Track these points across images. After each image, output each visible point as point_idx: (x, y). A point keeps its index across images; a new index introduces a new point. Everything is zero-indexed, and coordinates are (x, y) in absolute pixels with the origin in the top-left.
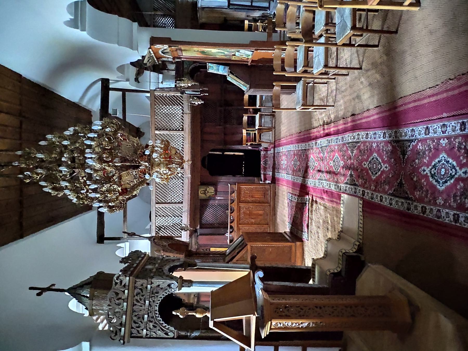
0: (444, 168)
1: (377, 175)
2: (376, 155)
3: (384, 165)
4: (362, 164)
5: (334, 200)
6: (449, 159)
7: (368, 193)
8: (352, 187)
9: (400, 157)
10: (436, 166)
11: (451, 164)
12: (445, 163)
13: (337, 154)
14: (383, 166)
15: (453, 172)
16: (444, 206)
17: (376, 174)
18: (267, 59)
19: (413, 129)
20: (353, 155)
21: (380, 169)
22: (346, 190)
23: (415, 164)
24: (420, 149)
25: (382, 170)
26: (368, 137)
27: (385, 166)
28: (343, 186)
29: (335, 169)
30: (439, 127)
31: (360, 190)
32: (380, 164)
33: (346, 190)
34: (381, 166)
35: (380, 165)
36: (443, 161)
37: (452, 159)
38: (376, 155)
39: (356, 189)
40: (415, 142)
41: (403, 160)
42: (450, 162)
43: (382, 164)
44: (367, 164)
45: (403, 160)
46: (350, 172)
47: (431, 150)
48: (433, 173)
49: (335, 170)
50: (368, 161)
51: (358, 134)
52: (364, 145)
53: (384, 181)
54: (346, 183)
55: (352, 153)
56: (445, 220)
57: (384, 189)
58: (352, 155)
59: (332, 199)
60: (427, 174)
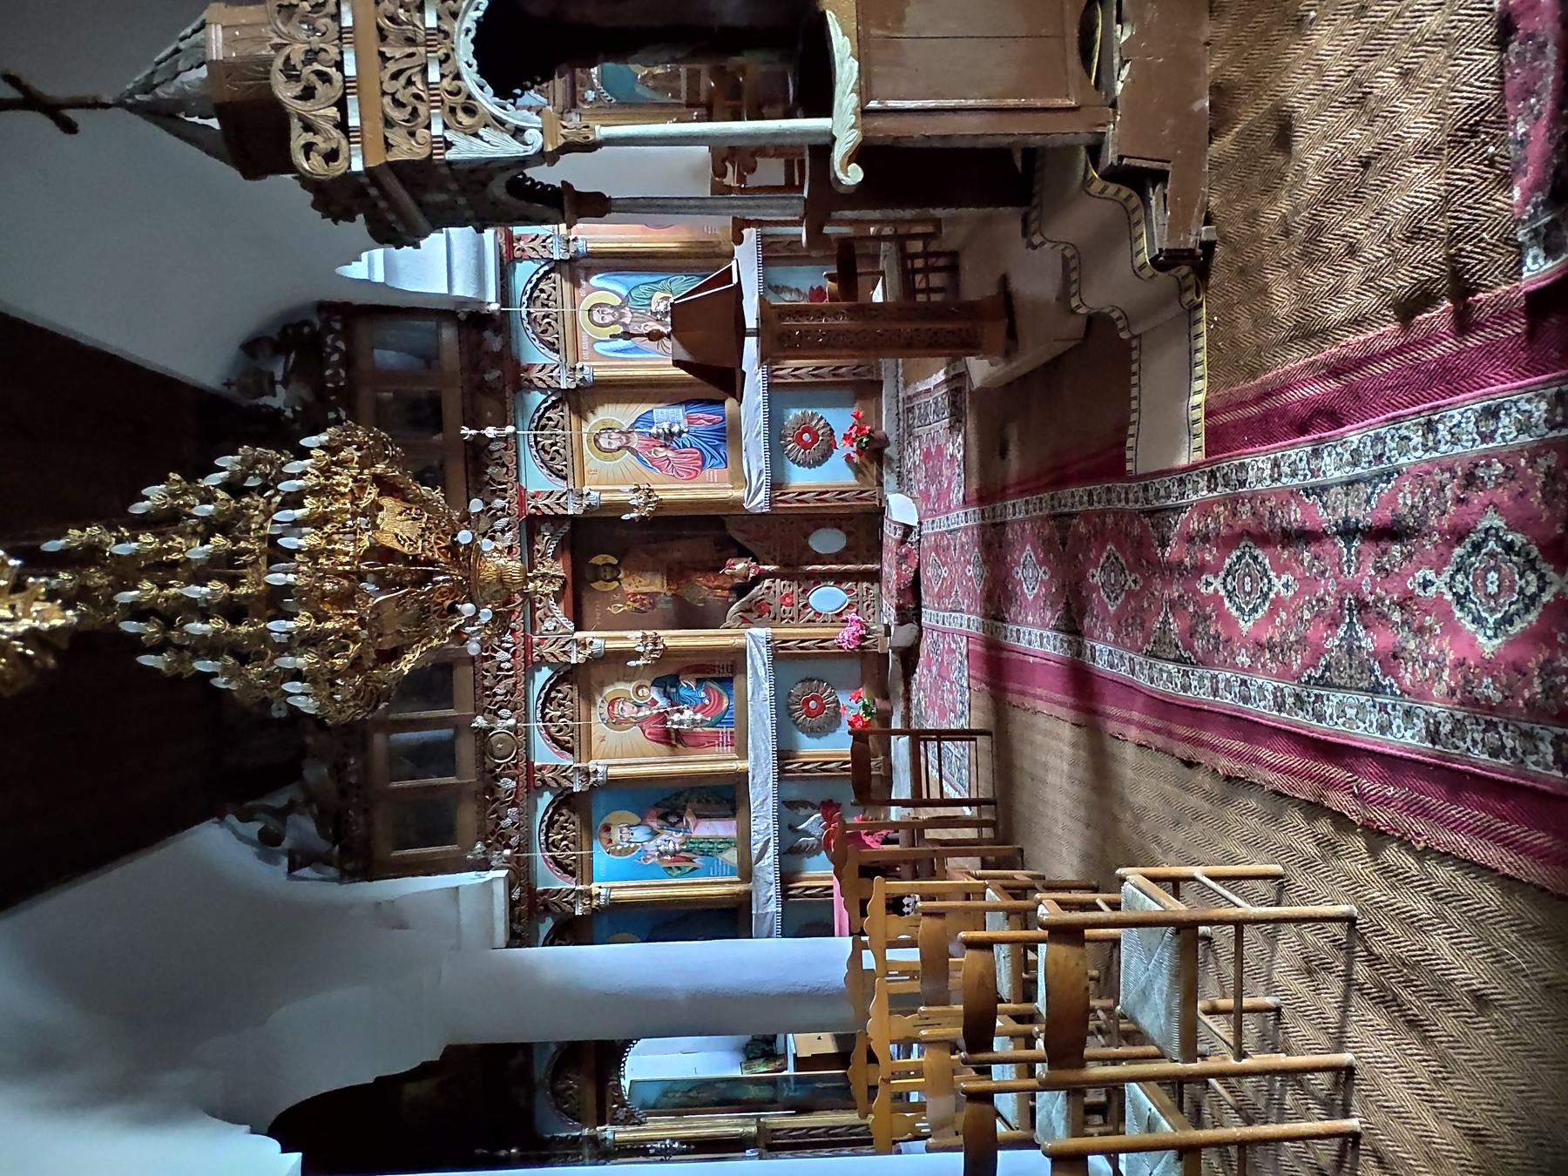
0: (1489, 596)
1: (1105, 555)
2: (1242, 623)
3: (1216, 591)
4: (1141, 583)
5: (1254, 410)
6: (1473, 627)
7: (1081, 503)
8: (1157, 504)
9: (1365, 628)
10: (1520, 605)
11: (1470, 611)
12: (1484, 615)
13: (1245, 626)
14: (1220, 588)
15: (1527, 583)
16: (1023, 521)
17: (1108, 558)
18: (156, 123)
19: (1383, 733)
20: (1163, 614)
21: (1227, 576)
22: (1182, 482)
23: (1313, 607)
24: (1296, 652)
25: (1448, 570)
26: (1274, 694)
27: (1211, 589)
28: (1120, 501)
29: (1117, 559)
30: (1331, 718)
31: (1136, 502)
32: (1230, 595)
33: (1182, 482)
34: (1225, 587)
35: (1229, 587)
36: (1491, 621)
37: (1230, 614)
38: (1242, 623)
39: (1147, 501)
40: (1309, 676)
41: (1351, 620)
42: (1470, 617)
43: (1222, 593)
44: (1130, 582)
45: (1351, 620)
46: (1167, 555)
47: (1541, 669)
48: (1532, 577)
49: (1258, 552)
50: (1272, 602)
51: (1383, 729)
52: (1288, 666)
53: (1089, 543)
54: (1178, 510)
55: (1165, 622)
56: (1462, 414)
57: (1088, 522)
58: (1351, 624)
59: (1266, 405)
60: (1278, 577)
